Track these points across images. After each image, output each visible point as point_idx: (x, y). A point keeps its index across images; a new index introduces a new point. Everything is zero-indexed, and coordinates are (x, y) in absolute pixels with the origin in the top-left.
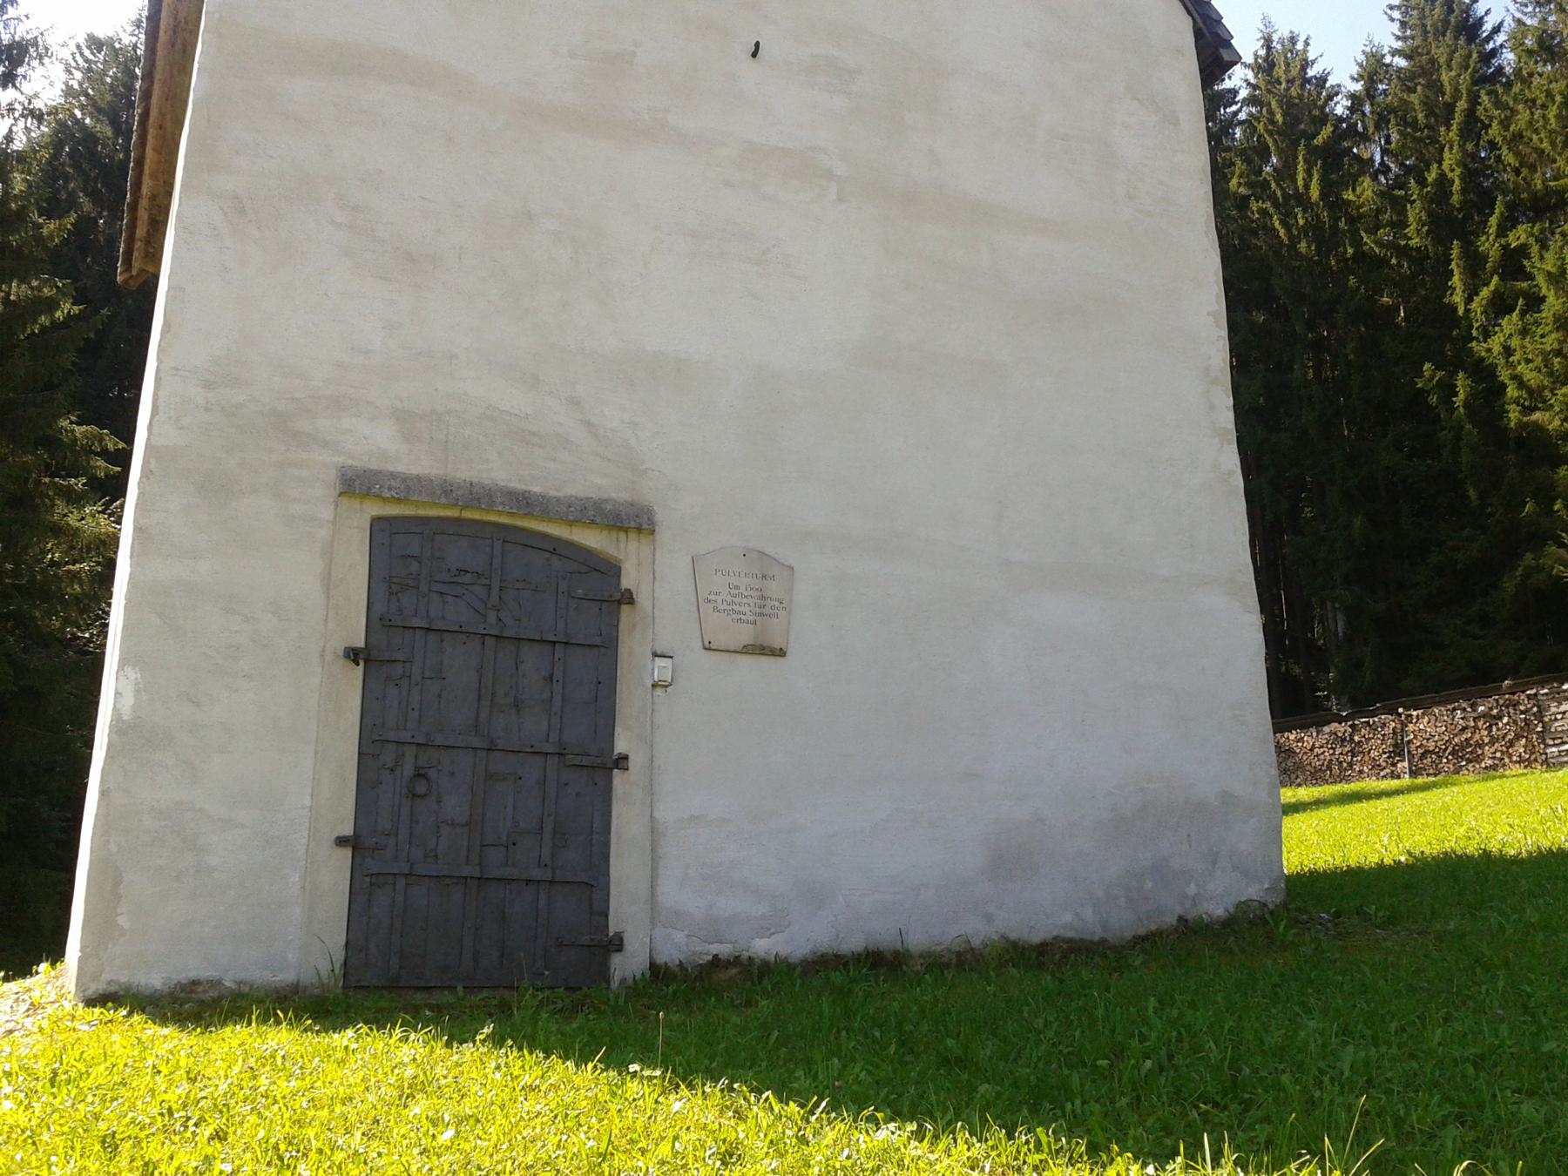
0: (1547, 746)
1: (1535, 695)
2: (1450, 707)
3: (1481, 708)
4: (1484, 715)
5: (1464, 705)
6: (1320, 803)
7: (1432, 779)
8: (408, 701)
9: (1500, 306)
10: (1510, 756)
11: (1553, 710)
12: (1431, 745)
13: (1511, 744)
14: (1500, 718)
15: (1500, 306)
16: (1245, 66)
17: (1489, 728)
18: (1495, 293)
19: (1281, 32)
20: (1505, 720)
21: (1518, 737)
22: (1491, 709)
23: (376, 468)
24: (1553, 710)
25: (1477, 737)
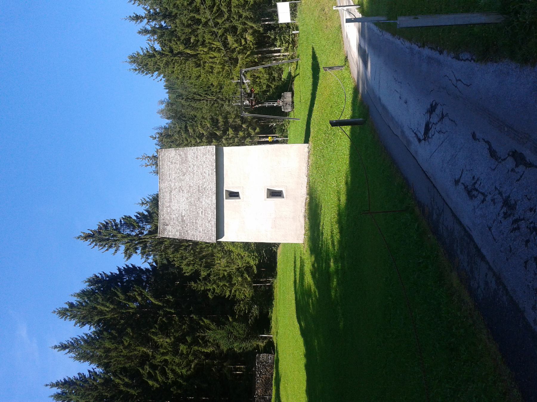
0: (269, 362)
1: (258, 363)
2: (256, 383)
3: (258, 376)
4: (260, 375)
5: (257, 380)
6: (295, 271)
7: (274, 370)
8: (277, 343)
9: (164, 373)
10: (270, 371)
11: (261, 360)
12: (264, 390)
13: (267, 370)
14: (261, 371)
15: (164, 373)
16: (116, 252)
17: (263, 375)
18: (160, 373)
19: (154, 133)
20: (262, 370)
21: (266, 368)
22: (259, 373)
23: (177, 236)
24: (261, 360)
25: (264, 378)
